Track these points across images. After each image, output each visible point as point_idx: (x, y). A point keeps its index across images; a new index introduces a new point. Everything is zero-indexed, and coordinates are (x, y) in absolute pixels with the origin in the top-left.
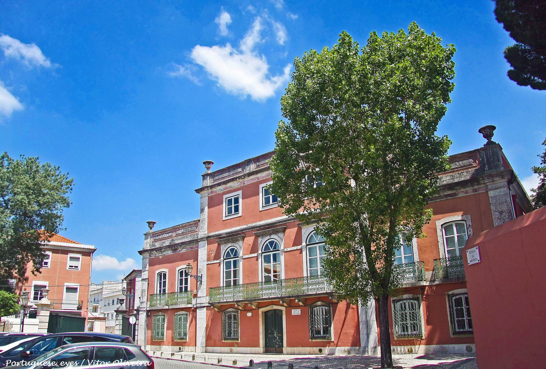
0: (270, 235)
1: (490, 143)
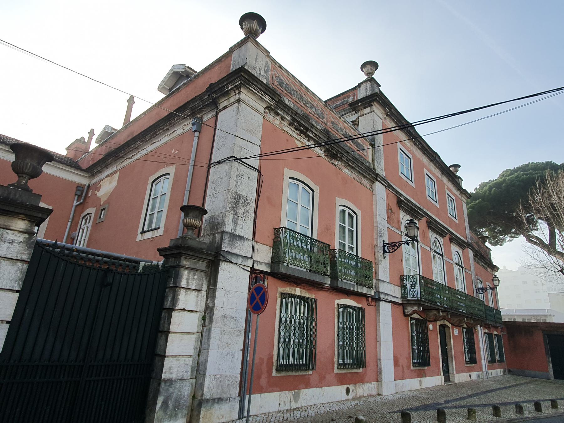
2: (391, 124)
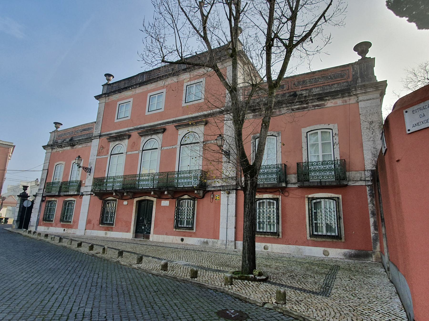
0: (152, 134)
1: (364, 59)
2: (308, 39)
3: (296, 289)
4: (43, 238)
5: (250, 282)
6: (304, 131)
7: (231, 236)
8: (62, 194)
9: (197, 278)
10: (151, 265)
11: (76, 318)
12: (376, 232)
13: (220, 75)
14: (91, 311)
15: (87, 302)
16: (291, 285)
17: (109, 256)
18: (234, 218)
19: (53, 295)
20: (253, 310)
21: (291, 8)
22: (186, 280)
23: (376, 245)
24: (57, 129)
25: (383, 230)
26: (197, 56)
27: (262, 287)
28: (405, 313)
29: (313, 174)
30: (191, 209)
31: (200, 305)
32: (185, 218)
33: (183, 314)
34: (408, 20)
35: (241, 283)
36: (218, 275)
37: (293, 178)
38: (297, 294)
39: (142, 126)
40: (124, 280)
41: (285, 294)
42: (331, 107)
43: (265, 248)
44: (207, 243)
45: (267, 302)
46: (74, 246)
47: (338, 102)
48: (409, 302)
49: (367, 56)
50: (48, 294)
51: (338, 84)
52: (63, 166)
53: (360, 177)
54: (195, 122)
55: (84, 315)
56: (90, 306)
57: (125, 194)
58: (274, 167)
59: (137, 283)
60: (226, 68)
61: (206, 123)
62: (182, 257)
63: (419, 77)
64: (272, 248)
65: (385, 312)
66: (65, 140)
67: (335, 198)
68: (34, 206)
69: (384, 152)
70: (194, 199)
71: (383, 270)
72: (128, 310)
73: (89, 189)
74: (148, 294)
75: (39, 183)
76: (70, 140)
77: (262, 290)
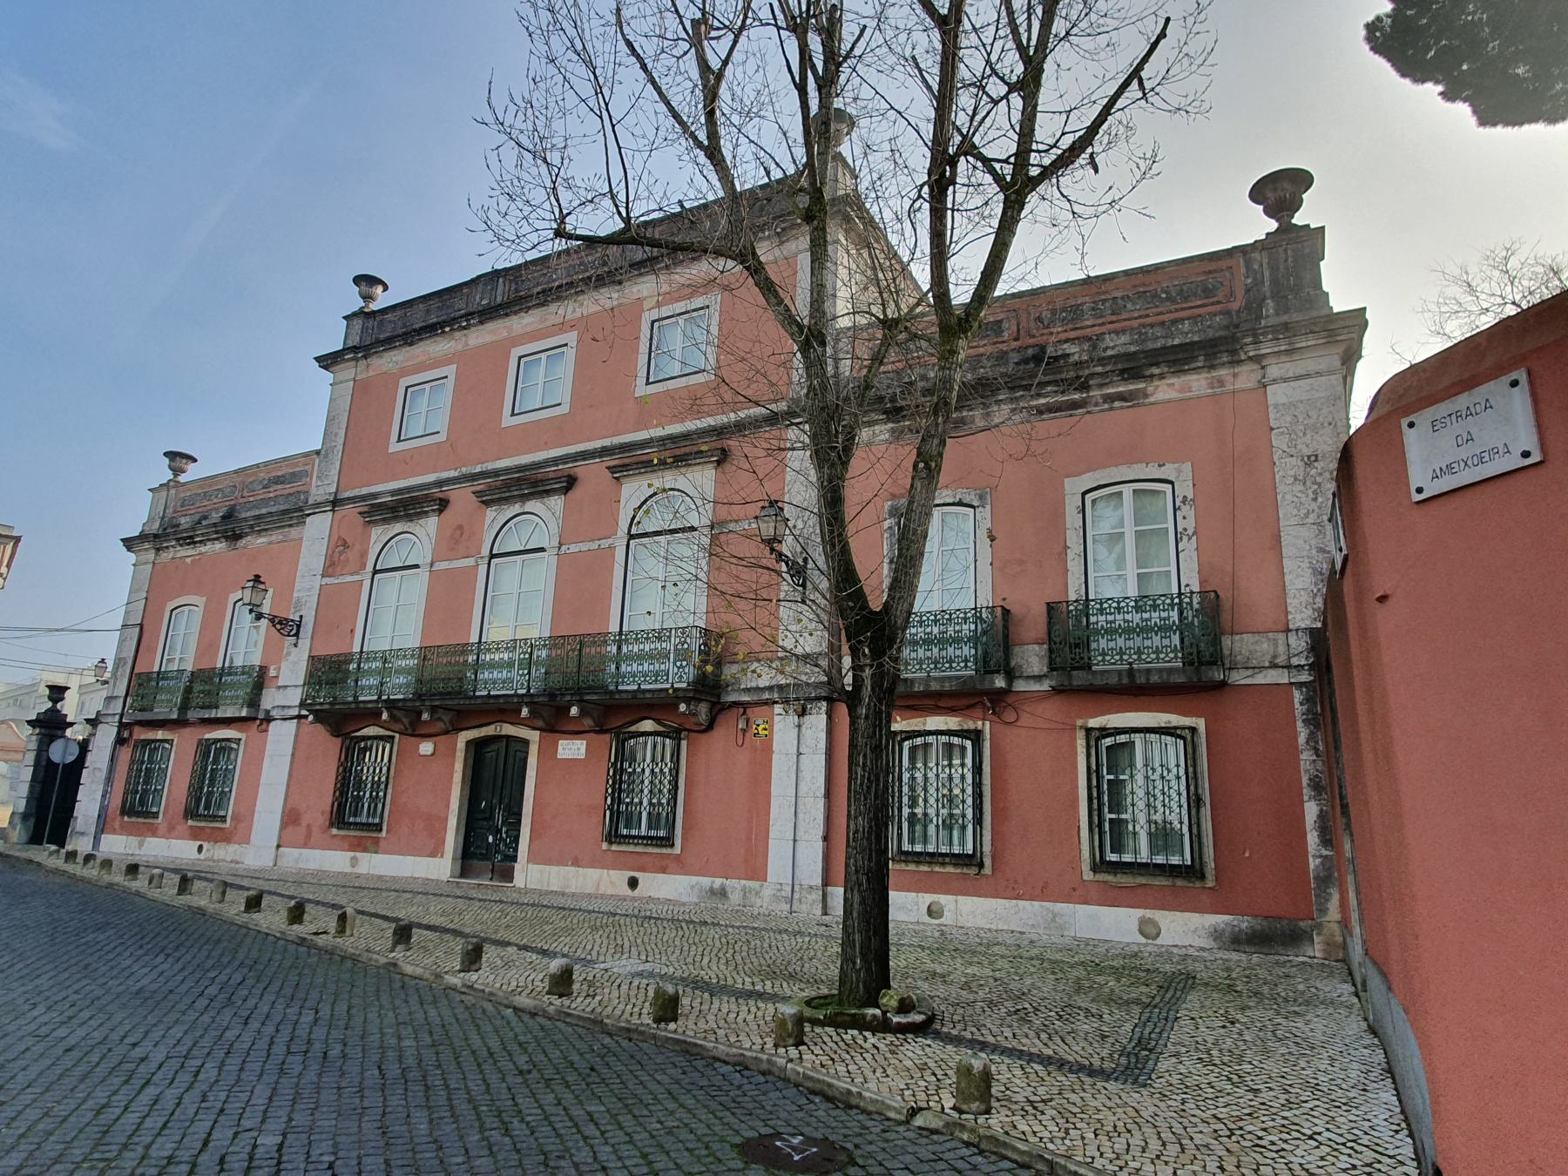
0: (524, 498)
1: (1287, 230)
2: (1083, 159)
3: (1031, 1058)
4: (118, 878)
5: (867, 1034)
6: (1074, 486)
7: (811, 869)
8: (193, 715)
9: (675, 1020)
10: (514, 977)
11: (222, 1170)
12: (1325, 853)
13: (768, 288)
14: (281, 1146)
15: (265, 1112)
16: (1015, 1043)
17: (362, 944)
18: (821, 803)
19: (143, 1087)
20: (870, 1138)
21: (1022, 49)
22: (636, 1030)
23: (1327, 900)
24: (176, 475)
25: (1348, 846)
26: (685, 218)
27: (910, 1054)
28: (1409, 1140)
29: (1103, 643)
30: (666, 770)
31: (680, 1120)
32: (645, 802)
33: (615, 1151)
34: (1441, 94)
35: (836, 1038)
36: (753, 1009)
37: (1032, 658)
38: (1033, 1076)
39: (490, 466)
40: (410, 1029)
41: (987, 1077)
42: (1170, 401)
43: (930, 912)
44: (723, 893)
45: (924, 1105)
46: (234, 907)
47: (1195, 385)
48: (1420, 1099)
49: (1298, 219)
50: (126, 1082)
51: (1194, 319)
52: (198, 613)
53: (1267, 655)
54: (680, 452)
55: (251, 1159)
56: (275, 1125)
57: (425, 716)
58: (965, 619)
59: (457, 1043)
60: (786, 255)
61: (723, 457)
62: (627, 945)
63: (1483, 296)
64: (957, 911)
65: (1341, 1140)
66: (205, 518)
67: (1183, 728)
68: (90, 758)
69: (1338, 566)
70: (676, 734)
71: (1348, 988)
72: (417, 1140)
73: (294, 697)
74: (493, 1078)
75: (107, 675)
76: (223, 517)
77: (909, 1063)
